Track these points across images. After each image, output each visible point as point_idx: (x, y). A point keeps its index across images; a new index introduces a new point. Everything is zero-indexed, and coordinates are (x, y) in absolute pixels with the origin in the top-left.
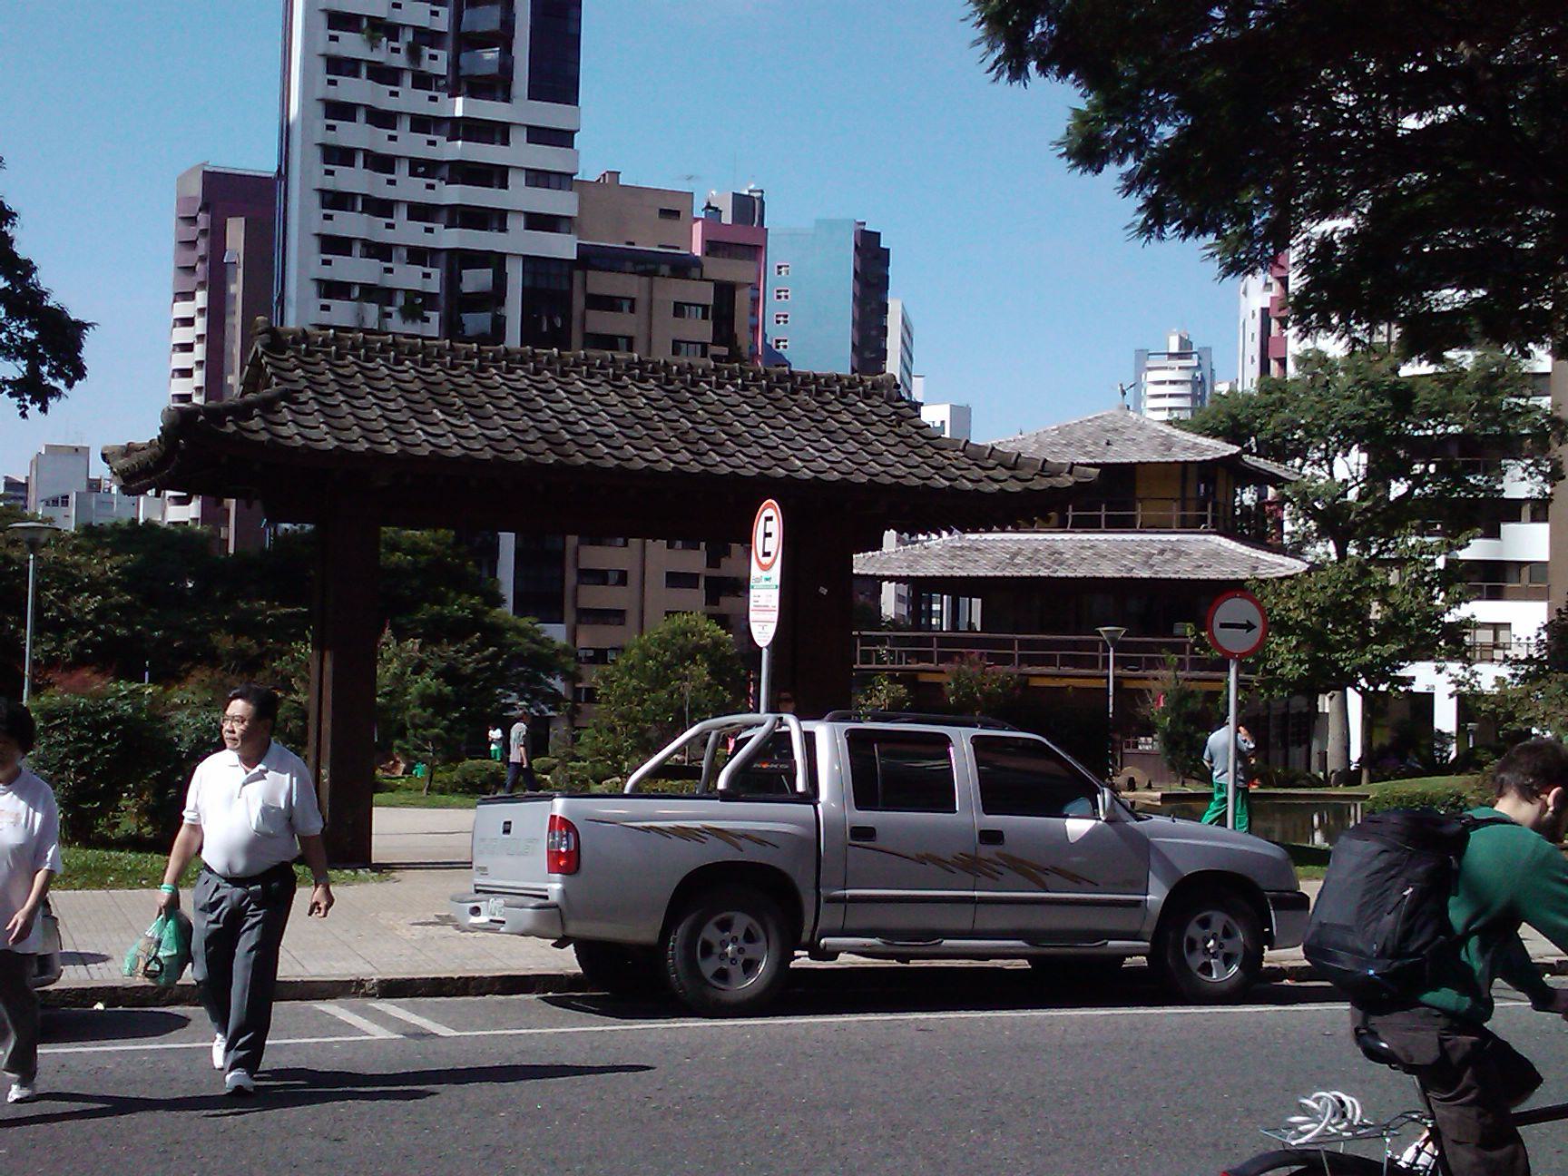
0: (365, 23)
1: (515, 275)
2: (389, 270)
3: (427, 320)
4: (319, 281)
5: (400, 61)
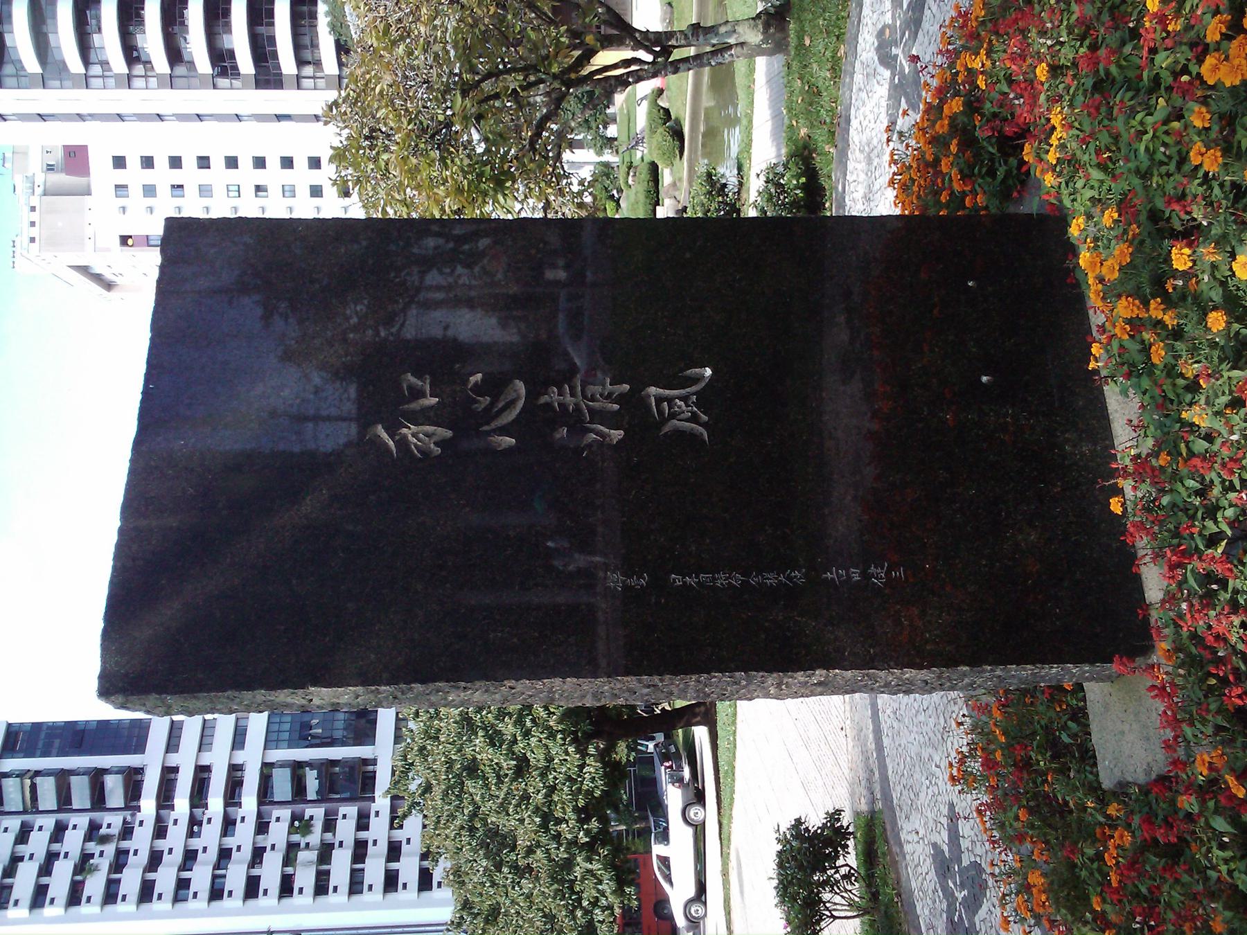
0: (79, 878)
1: (277, 755)
2: (273, 847)
3: (311, 818)
4: (281, 897)
5: (110, 849)
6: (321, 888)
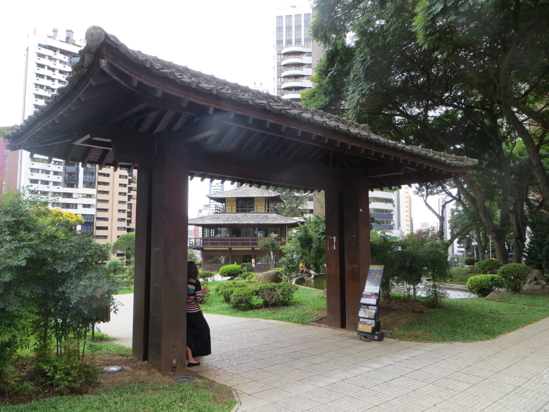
4: (37, 53)
6: (32, 170)
